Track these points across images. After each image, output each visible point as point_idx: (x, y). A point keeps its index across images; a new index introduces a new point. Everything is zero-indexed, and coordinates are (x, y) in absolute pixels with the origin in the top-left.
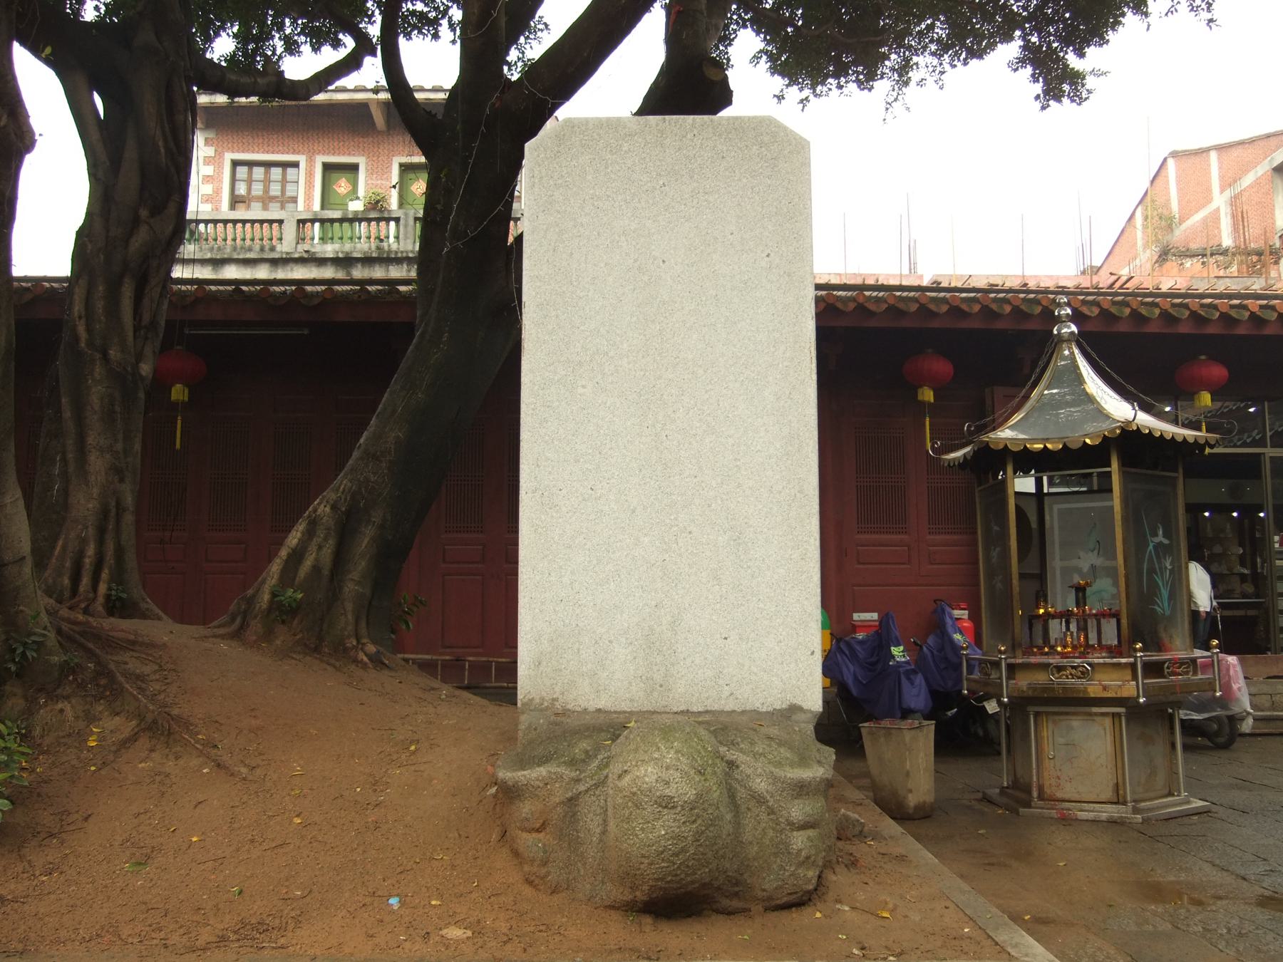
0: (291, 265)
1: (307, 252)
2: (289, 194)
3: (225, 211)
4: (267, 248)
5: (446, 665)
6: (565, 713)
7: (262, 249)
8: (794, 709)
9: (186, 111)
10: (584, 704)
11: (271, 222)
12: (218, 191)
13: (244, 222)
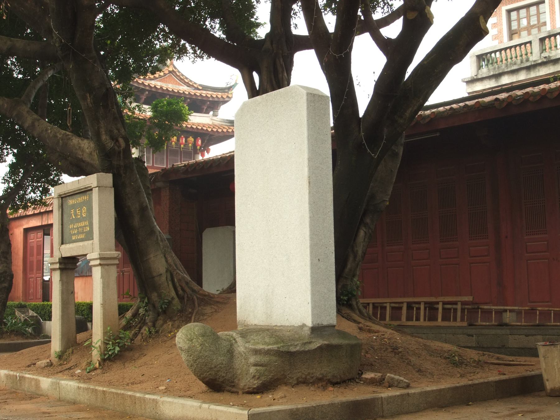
0: (538, 68)
1: (545, 57)
2: (542, 21)
3: (507, 43)
4: (524, 60)
5: (526, 312)
6: (247, 325)
7: (522, 62)
8: (304, 325)
9: (283, 72)
10: (252, 323)
11: (525, 44)
12: (500, 32)
13: (520, 45)
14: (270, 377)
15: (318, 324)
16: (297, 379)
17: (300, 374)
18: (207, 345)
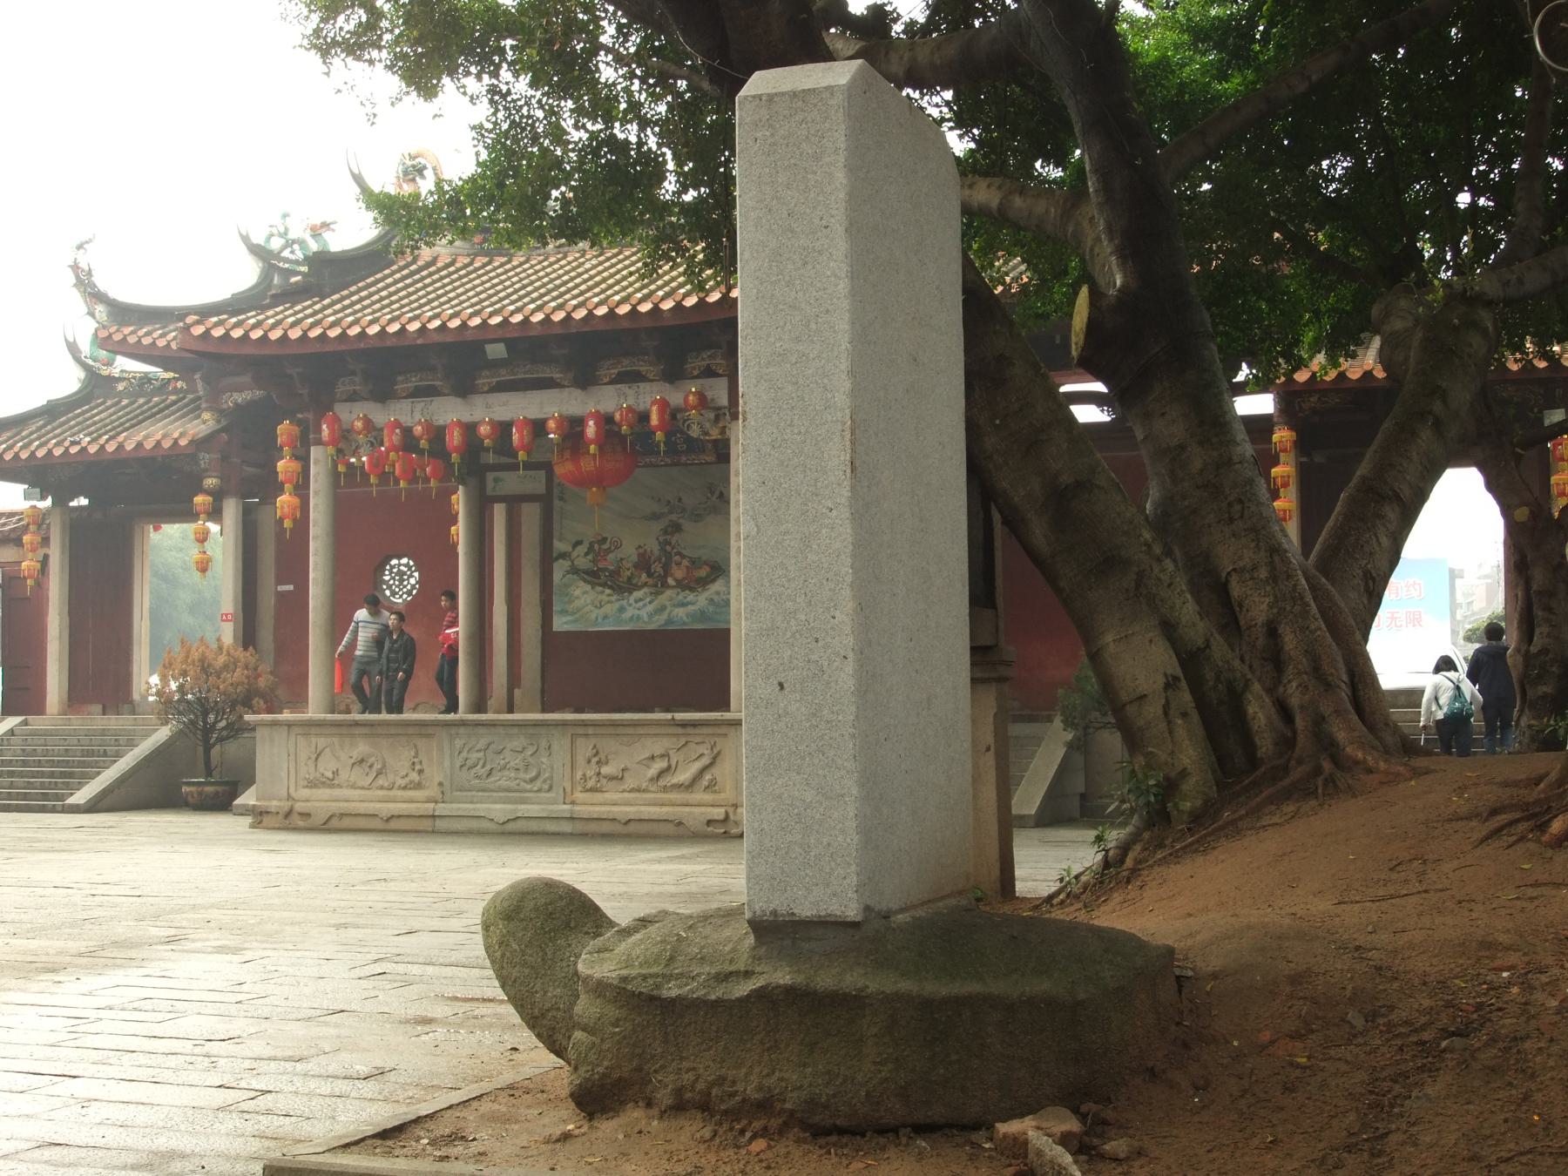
14: (600, 1070)
15: (774, 913)
16: (679, 1092)
17: (690, 1076)
18: (515, 946)
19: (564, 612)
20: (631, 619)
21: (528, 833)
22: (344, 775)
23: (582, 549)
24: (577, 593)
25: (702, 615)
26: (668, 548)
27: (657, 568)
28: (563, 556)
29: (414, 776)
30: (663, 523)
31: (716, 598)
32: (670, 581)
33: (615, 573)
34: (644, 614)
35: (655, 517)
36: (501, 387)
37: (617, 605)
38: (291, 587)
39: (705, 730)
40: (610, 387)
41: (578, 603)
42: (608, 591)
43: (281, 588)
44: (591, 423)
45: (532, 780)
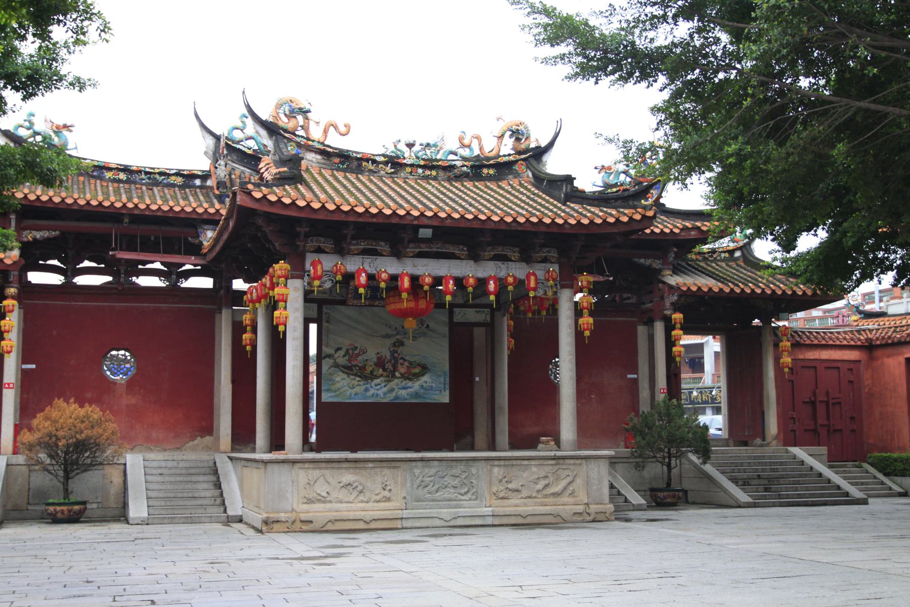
19: (329, 390)
20: (373, 395)
21: (507, 525)
22: (334, 495)
23: (342, 353)
24: (338, 379)
25: (417, 395)
26: (396, 355)
27: (389, 366)
28: (329, 356)
29: (386, 493)
30: (393, 340)
31: (425, 385)
32: (397, 374)
33: (363, 368)
34: (380, 392)
35: (388, 336)
36: (421, 255)
37: (364, 387)
38: (34, 366)
39: (568, 461)
40: (492, 263)
41: (338, 385)
42: (358, 379)
43: (635, 376)
44: (491, 282)
45: (466, 493)
